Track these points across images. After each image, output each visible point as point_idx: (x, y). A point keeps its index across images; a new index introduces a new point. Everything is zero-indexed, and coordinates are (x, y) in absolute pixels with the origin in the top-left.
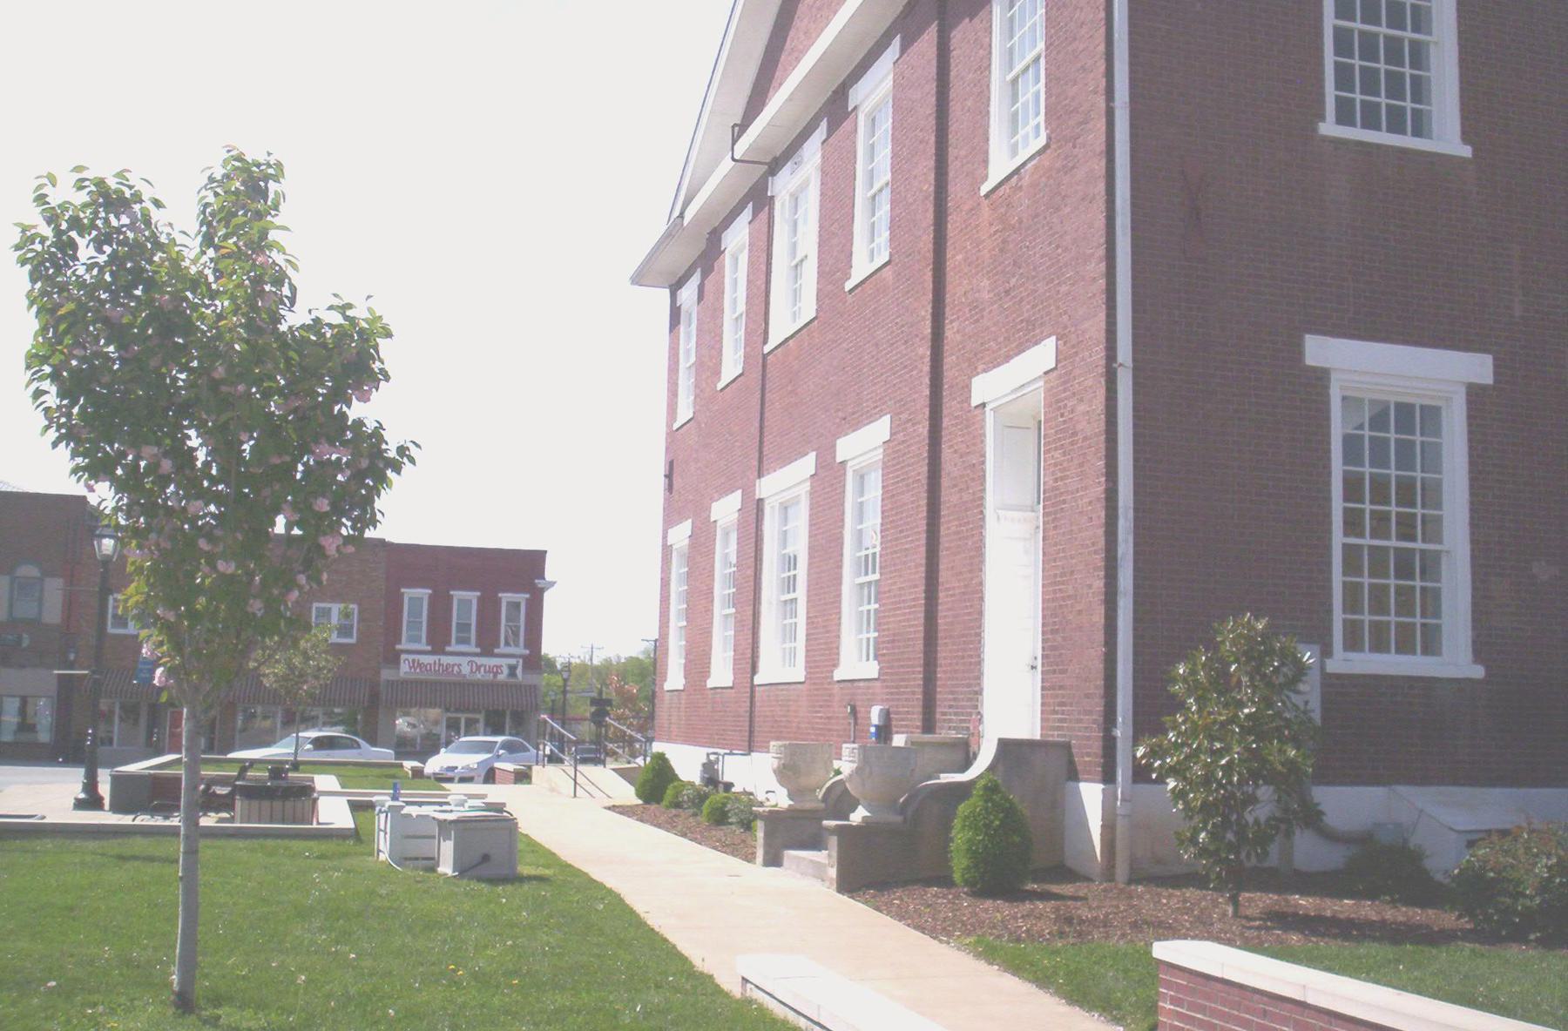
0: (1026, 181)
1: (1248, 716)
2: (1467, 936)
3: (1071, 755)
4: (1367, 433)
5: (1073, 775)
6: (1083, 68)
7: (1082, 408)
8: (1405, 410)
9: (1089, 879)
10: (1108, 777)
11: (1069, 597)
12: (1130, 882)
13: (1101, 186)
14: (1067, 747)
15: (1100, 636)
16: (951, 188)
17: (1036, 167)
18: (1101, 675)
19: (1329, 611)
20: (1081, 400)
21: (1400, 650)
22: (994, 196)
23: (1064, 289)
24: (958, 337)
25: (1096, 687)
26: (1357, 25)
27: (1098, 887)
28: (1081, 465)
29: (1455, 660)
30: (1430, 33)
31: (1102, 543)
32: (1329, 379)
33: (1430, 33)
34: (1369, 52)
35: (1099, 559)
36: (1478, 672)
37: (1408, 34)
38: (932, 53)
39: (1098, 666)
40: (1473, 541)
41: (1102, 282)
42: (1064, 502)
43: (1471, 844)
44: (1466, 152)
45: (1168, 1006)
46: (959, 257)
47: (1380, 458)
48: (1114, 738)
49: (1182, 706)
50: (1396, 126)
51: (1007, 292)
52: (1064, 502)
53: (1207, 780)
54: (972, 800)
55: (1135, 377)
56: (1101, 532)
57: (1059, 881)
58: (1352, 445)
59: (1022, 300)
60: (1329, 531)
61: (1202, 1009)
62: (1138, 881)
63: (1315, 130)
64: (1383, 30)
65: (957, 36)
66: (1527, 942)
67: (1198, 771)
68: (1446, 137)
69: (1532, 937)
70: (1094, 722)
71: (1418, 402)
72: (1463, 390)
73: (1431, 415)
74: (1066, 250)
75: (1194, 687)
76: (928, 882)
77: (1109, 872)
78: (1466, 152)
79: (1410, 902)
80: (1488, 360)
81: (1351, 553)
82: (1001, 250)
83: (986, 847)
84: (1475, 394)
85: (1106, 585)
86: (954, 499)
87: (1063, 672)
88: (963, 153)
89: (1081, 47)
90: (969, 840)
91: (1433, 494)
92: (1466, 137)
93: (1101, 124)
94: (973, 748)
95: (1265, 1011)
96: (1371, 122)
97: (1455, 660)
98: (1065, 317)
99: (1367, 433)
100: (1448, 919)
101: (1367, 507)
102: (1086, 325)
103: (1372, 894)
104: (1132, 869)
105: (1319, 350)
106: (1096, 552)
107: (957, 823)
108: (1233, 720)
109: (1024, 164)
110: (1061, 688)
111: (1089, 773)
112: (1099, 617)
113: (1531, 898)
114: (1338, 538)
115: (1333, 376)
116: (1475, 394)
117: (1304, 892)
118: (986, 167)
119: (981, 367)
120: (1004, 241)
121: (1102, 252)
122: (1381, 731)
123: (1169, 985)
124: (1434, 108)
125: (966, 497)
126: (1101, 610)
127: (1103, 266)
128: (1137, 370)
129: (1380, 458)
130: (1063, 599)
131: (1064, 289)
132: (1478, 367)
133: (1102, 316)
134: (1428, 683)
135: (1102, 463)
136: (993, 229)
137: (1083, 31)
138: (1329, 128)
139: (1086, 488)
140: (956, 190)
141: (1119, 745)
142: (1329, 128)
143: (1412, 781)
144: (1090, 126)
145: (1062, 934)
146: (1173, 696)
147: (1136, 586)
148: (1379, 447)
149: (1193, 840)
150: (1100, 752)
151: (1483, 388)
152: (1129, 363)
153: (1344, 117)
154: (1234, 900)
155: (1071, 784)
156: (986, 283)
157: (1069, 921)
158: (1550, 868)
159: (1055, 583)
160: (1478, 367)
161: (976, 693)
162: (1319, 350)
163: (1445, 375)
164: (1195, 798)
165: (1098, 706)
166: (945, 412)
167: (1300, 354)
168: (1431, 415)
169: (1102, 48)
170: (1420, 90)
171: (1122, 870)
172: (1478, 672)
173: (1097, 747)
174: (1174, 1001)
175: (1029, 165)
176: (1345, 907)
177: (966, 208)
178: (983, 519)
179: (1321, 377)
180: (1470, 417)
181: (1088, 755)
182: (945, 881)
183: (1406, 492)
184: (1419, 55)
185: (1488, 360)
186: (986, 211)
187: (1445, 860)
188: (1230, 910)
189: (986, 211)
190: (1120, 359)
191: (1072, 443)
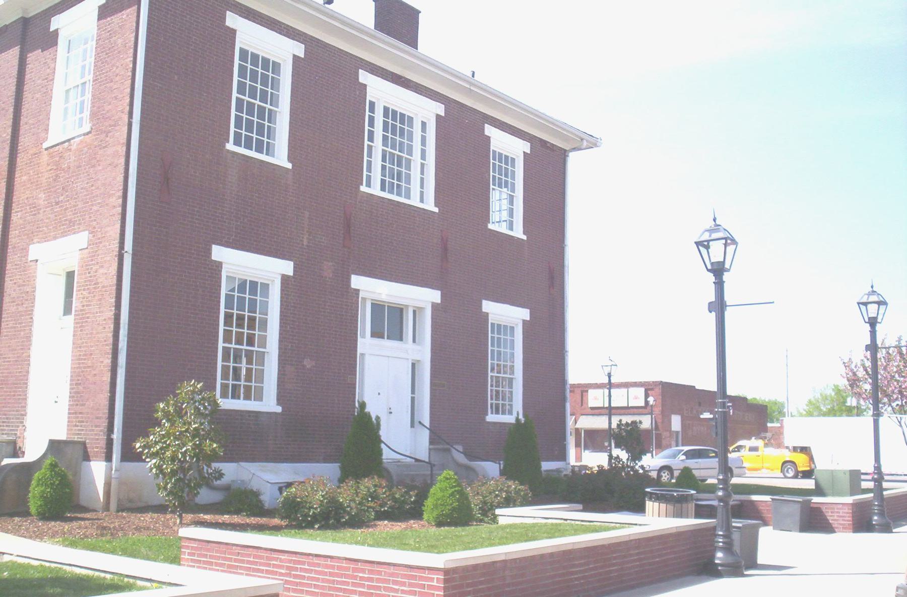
0: (74, 147)
1: (195, 428)
2: (287, 527)
3: (85, 447)
4: (236, 294)
5: (87, 458)
6: (116, 98)
7: (101, 271)
8: (254, 284)
9: (94, 511)
10: (109, 458)
11: (89, 367)
12: (118, 511)
13: (123, 160)
14: (84, 444)
15: (107, 388)
16: (21, 139)
17: (81, 141)
18: (107, 407)
19: (215, 379)
20: (102, 267)
21: (233, 397)
22: (51, 150)
23: (95, 208)
24: (21, 222)
25: (104, 414)
26: (247, 98)
27: (101, 515)
28: (100, 300)
29: (269, 403)
30: (277, 107)
31: (111, 340)
33: (277, 107)
34: (250, 112)
35: (109, 349)
36: (279, 409)
37: (268, 106)
38: (15, 62)
39: (106, 403)
40: (280, 349)
41: (119, 209)
42: (88, 318)
43: (280, 490)
44: (289, 166)
45: (187, 557)
46: (24, 178)
47: (241, 307)
48: (112, 440)
49: (158, 424)
50: (259, 150)
51: (57, 203)
52: (88, 318)
53: (173, 459)
54: (43, 471)
55: (133, 258)
56: (111, 335)
57: (81, 512)
58: (229, 298)
59: (66, 209)
60: (217, 340)
61: (205, 556)
62: (123, 511)
63: (224, 146)
64: (257, 102)
65: (32, 57)
66: (313, 528)
67: (168, 454)
68: (281, 157)
69: (316, 526)
70: (101, 431)
71: (260, 281)
72: (280, 277)
73: (266, 287)
74: (98, 188)
75: (167, 415)
76: (12, 515)
77: (107, 507)
78: (289, 166)
79: (255, 515)
80: (291, 264)
81: (226, 351)
82: (55, 180)
83: (51, 495)
84: (285, 279)
85: (112, 362)
86: (13, 309)
87: (83, 405)
88: (31, 122)
89: (115, 86)
90: (43, 492)
91: (264, 324)
92: (290, 159)
93: (125, 129)
94: (19, 444)
96: (248, 146)
97: (269, 403)
98: (94, 223)
99: (236, 294)
100: (276, 521)
101: (234, 329)
102: (108, 229)
103: (238, 512)
104: (118, 505)
105: (219, 253)
106: (107, 345)
107: (34, 483)
108: (187, 431)
109: (73, 138)
110: (81, 413)
111: (96, 457)
112: (107, 378)
113: (316, 508)
114: (221, 344)
116: (285, 279)
117: (206, 513)
118: (47, 133)
119: (35, 241)
120: (57, 176)
121: (120, 193)
122: (243, 437)
123: (187, 547)
124: (276, 143)
125: (21, 309)
126: (109, 374)
127: (120, 201)
128: (134, 255)
129: (241, 307)
130: (85, 368)
131: (95, 208)
132: (287, 267)
133: (118, 226)
134: (257, 414)
135: (114, 300)
136: (50, 168)
137: (117, 78)
138: (230, 146)
139: (102, 312)
140: (25, 140)
141: (115, 442)
142: (230, 146)
143: (247, 460)
144: (117, 128)
145: (102, 535)
146: (157, 419)
147: (127, 363)
148: (241, 300)
149: (165, 488)
150: (104, 446)
151: (288, 277)
152: (131, 252)
153: (237, 143)
154: (181, 516)
155: (85, 463)
156: (42, 196)
157: (104, 528)
158: (323, 496)
159: (79, 359)
160: (287, 267)
161: (22, 415)
162: (219, 253)
163: (272, 270)
164: (167, 468)
165: (105, 424)
166: (8, 261)
167: (480, 306)
169: (128, 90)
170: (271, 134)
171: (113, 505)
172: (279, 409)
173: (103, 443)
174: (189, 554)
175: (76, 140)
176: (226, 518)
177: (31, 152)
178: (32, 322)
180: (282, 290)
181: (97, 448)
182: (26, 514)
184: (272, 117)
185: (291, 264)
186: (45, 157)
187: (270, 497)
188: (178, 521)
189: (45, 157)
190: (126, 249)
191: (95, 288)
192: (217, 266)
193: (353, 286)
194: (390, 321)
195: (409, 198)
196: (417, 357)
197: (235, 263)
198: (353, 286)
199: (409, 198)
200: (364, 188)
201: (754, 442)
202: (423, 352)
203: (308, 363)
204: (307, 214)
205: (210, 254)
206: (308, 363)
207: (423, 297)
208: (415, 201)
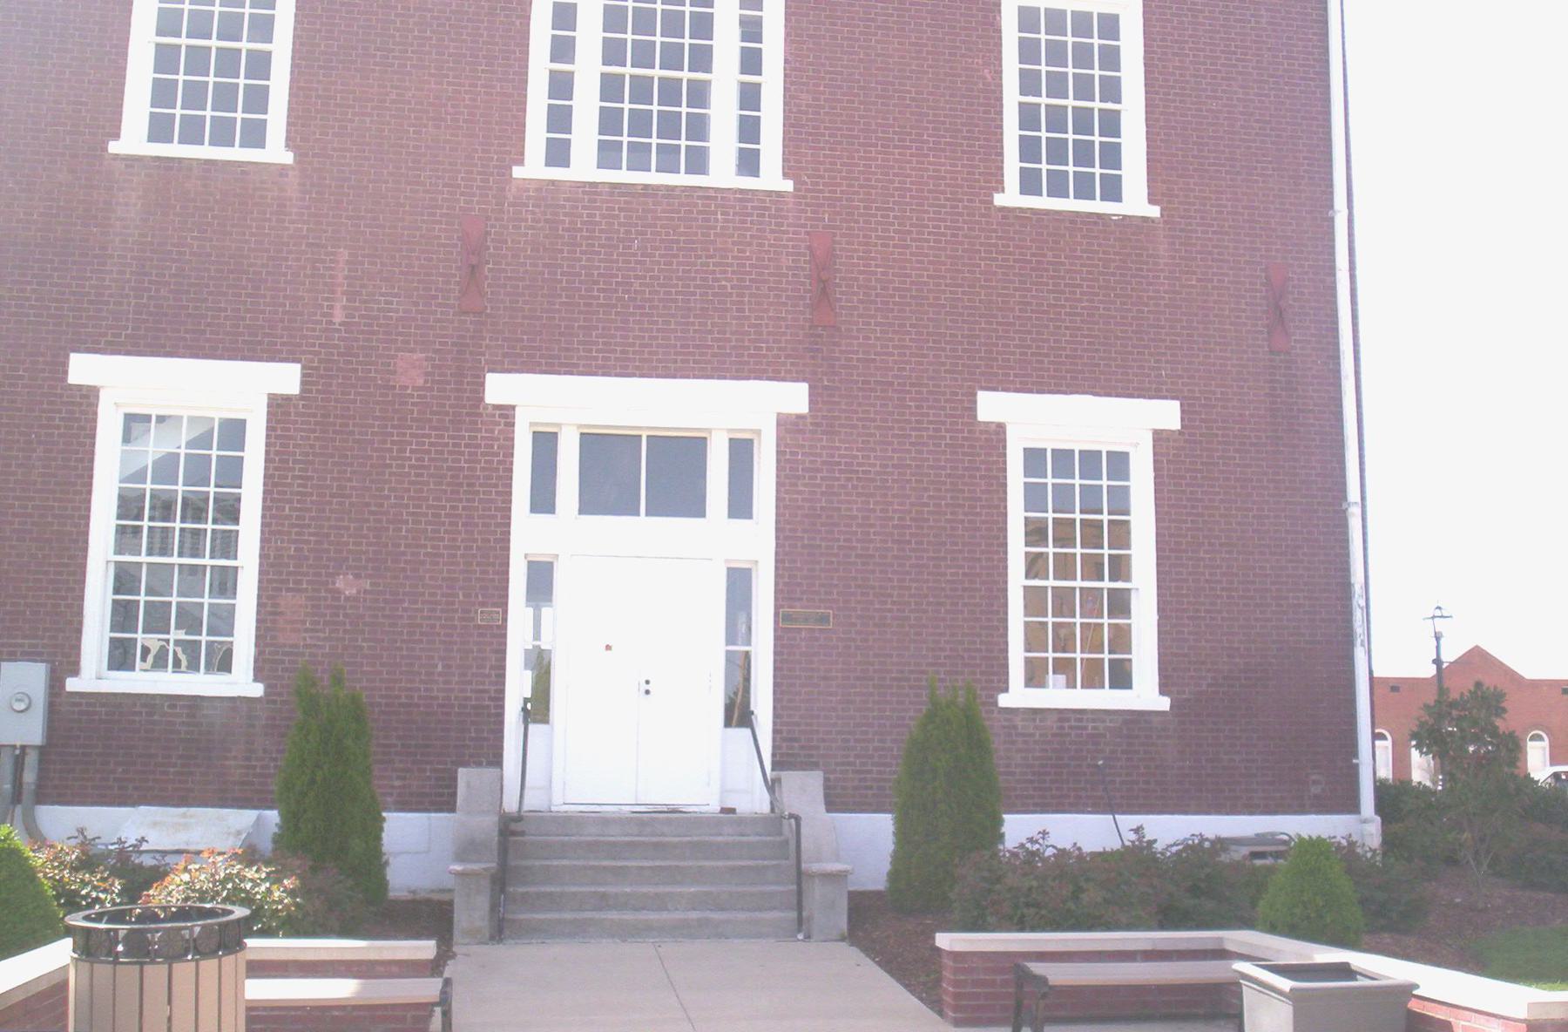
29: (1145, 694)
32: (97, 397)
64: (1070, 102)
73: (1119, 463)
78: (788, 186)
80: (803, 388)
95: (604, 896)
96: (1058, 190)
97: (1145, 694)
105: (991, 406)
115: (518, 411)
116: (1159, 437)
132: (1167, 414)
151: (287, 398)
160: (1167, 414)
162: (991, 406)
163: (244, 390)
167: (972, 409)
168: (1119, 463)
179: (88, 397)
183: (1092, 533)
185: (803, 388)
192: (87, 397)
193: (74, 378)
194: (645, 477)
195: (1118, 199)
196: (741, 559)
197: (1028, 420)
198: (74, 378)
199: (1118, 199)
200: (533, 167)
201: (1359, 850)
202: (755, 542)
203: (346, 585)
204: (344, 254)
205: (66, 373)
206: (346, 585)
207: (749, 409)
208: (722, 173)
